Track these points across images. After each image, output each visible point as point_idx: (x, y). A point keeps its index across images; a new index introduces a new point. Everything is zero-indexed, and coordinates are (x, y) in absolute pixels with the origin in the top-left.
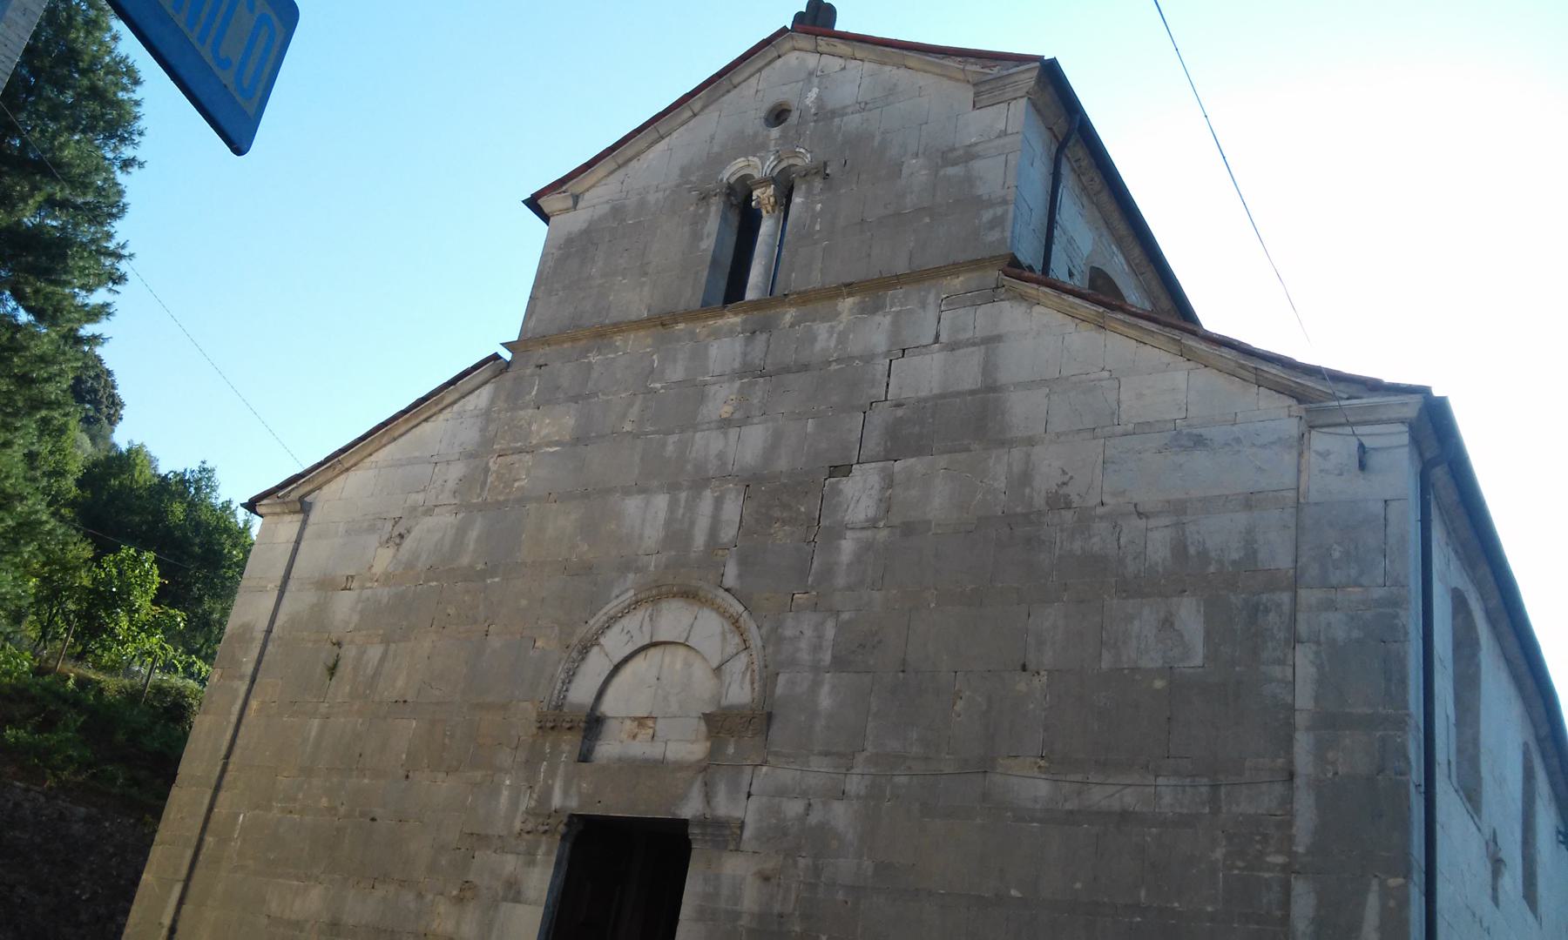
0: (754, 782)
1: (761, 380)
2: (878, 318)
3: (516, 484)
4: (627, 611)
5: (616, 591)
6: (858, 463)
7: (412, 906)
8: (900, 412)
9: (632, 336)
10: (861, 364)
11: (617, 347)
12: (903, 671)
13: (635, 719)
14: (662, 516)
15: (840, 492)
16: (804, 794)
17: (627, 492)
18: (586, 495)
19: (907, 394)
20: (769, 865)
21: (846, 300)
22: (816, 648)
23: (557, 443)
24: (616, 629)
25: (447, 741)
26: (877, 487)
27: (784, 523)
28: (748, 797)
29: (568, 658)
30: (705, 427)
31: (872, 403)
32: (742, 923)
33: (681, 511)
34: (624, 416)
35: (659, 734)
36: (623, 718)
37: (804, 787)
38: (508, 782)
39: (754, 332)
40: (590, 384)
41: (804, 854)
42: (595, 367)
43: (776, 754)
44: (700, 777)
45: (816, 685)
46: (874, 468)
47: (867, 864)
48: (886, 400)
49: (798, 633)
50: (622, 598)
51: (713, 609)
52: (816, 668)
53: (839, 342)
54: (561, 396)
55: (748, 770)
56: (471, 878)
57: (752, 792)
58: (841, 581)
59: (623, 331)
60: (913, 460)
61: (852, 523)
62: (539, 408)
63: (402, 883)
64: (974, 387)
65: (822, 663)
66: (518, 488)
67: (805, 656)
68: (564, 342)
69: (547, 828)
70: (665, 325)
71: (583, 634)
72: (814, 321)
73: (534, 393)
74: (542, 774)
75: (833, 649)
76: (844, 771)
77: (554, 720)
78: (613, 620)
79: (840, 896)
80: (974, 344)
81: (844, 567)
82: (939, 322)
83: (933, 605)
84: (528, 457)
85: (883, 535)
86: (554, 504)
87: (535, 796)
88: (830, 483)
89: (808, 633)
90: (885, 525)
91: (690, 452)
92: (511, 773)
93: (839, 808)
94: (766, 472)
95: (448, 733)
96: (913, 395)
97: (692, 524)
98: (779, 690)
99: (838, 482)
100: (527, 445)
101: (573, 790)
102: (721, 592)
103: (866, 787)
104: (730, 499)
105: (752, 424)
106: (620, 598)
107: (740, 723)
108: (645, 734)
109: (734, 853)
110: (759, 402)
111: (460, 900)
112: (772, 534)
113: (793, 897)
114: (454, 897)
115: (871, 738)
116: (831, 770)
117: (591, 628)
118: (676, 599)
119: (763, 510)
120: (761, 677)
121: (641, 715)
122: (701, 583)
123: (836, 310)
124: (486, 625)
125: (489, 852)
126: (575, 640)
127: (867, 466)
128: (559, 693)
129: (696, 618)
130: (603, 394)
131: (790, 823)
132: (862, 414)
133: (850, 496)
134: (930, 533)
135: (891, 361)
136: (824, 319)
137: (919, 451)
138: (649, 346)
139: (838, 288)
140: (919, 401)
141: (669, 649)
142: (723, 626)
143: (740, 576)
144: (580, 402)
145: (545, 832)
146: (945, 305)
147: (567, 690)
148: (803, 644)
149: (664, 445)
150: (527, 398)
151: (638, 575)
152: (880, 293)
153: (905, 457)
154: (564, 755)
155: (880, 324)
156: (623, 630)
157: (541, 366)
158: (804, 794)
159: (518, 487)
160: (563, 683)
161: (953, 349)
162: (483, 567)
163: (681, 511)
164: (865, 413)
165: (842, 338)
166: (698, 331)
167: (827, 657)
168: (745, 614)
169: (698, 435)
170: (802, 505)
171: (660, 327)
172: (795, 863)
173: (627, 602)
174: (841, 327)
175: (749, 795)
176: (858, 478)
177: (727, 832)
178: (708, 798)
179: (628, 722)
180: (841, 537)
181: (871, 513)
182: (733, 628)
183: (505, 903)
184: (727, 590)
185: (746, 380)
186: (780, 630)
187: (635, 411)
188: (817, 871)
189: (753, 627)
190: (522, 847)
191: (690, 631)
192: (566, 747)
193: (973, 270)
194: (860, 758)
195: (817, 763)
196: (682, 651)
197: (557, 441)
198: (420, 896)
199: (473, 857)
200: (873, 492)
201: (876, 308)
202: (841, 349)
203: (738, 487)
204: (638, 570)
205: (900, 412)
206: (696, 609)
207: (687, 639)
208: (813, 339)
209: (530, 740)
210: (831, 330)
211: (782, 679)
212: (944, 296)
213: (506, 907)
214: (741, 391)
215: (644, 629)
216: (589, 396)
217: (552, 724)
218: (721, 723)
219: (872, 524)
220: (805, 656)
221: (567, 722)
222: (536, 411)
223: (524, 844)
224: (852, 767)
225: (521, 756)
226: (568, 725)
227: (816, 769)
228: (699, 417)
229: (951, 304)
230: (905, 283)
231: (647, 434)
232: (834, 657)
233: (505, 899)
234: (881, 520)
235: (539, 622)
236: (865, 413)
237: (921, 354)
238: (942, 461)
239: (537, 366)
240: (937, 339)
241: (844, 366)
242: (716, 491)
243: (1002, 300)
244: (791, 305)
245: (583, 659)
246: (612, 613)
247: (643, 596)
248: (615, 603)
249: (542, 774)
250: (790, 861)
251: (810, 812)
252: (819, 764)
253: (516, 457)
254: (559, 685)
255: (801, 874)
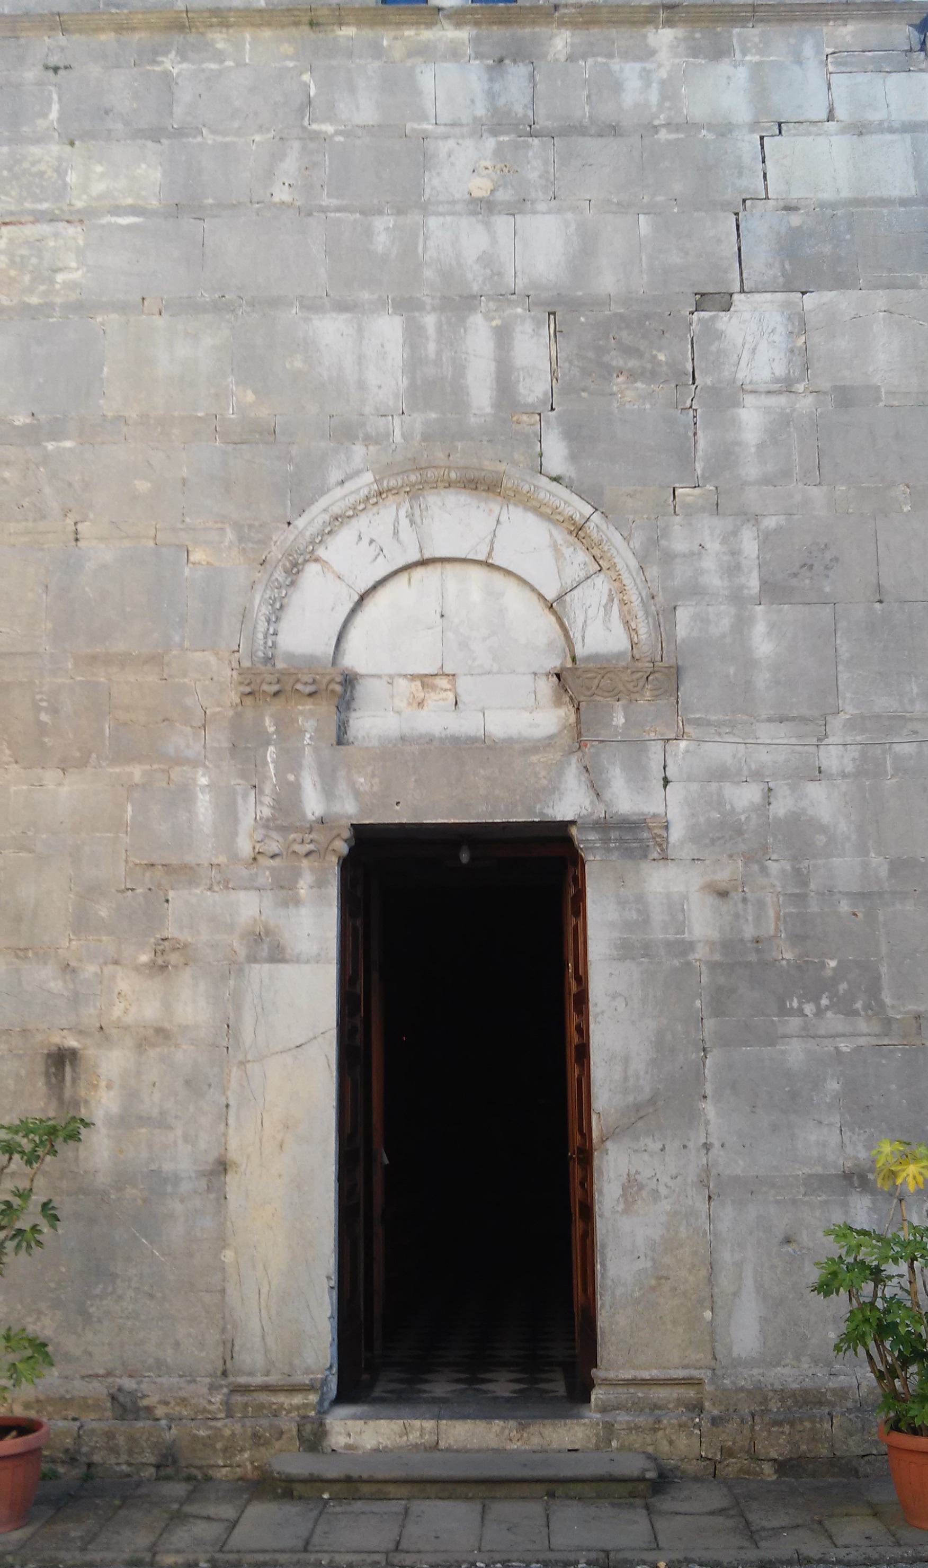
0: (669, 762)
1: (536, 141)
2: (724, 67)
3: (60, 277)
4: (361, 507)
5: (335, 475)
6: (742, 291)
7: (56, 985)
8: (795, 220)
9: (248, 36)
10: (711, 136)
11: (221, 52)
12: (881, 602)
13: (413, 677)
14: (396, 353)
15: (719, 336)
16: (757, 775)
17: (312, 307)
18: (220, 307)
19: (797, 193)
20: (723, 875)
21: (660, 31)
22: (733, 569)
23: (134, 210)
24: (346, 535)
25: (44, 717)
26: (781, 329)
27: (633, 376)
28: (665, 786)
29: (269, 580)
30: (441, 209)
31: (744, 201)
32: (697, 956)
33: (432, 347)
34: (270, 175)
35: (463, 698)
36: (391, 677)
37: (753, 767)
38: (203, 781)
39: (501, 61)
40: (178, 110)
41: (774, 857)
42: (179, 81)
43: (698, 723)
44: (574, 759)
45: (742, 624)
46: (772, 302)
47: (879, 864)
48: (767, 198)
49: (696, 548)
50: (350, 486)
51: (527, 508)
52: (737, 597)
53: (664, 97)
54: (120, 126)
55: (656, 749)
56: (171, 931)
57: (670, 777)
58: (751, 470)
59: (229, 26)
60: (834, 293)
61: (751, 383)
62: (72, 144)
63: (21, 954)
64: (905, 195)
65: (746, 591)
66: (65, 284)
67: (714, 581)
68: (98, 29)
69: (311, 847)
70: (318, 24)
71: (288, 543)
72: (610, 56)
73: (54, 115)
74: (271, 766)
75: (760, 571)
76: (814, 741)
77: (278, 682)
78: (339, 520)
79: (845, 907)
80: (892, 130)
81: (753, 450)
82: (829, 88)
83: (907, 508)
84: (71, 230)
85: (806, 403)
86: (156, 317)
87: (267, 800)
88: (699, 320)
89: (714, 546)
90: (806, 388)
91: (425, 249)
92: (204, 766)
93: (816, 792)
94: (580, 293)
95: (44, 704)
96: (811, 195)
97: (460, 369)
98: (681, 632)
99: (712, 319)
100: (66, 208)
101: (342, 787)
102: (544, 481)
103: (854, 760)
104: (523, 332)
105: (534, 212)
106: (347, 485)
107: (632, 681)
108: (439, 700)
109: (662, 862)
110: (540, 177)
111: (159, 968)
112: (613, 394)
113: (771, 913)
114: (145, 965)
115: (848, 695)
116: (794, 741)
117: (301, 533)
118: (451, 490)
119: (591, 355)
120: (647, 613)
121: (427, 672)
122: (502, 467)
123: (647, 45)
124: (70, 521)
125: (198, 891)
126: (275, 553)
127: (757, 297)
128: (266, 637)
129: (498, 521)
130: (214, 132)
131: (743, 818)
132: (734, 217)
133: (739, 341)
134: (881, 404)
135: (762, 138)
136: (626, 55)
137: (841, 282)
138: (287, 57)
139: (653, 9)
140: (822, 205)
141: (449, 567)
142: (551, 535)
143: (574, 457)
144: (163, 141)
145: (308, 854)
146: (837, 64)
147: (275, 634)
148: (709, 563)
149: (368, 232)
150: (41, 124)
151: (371, 448)
152: (719, 29)
153: (820, 288)
154: (308, 736)
155: (729, 78)
156: (360, 538)
157: (56, 69)
158: (757, 775)
159: (64, 282)
160: (269, 621)
161: (861, 134)
162: (28, 421)
163: (432, 347)
164: (737, 214)
165: (669, 92)
166: (385, 43)
167: (753, 583)
168: (596, 517)
169: (433, 222)
170: (660, 350)
171: (306, 28)
172: (764, 870)
173: (364, 492)
174: (663, 73)
175: (666, 781)
176: (746, 315)
177: (646, 835)
178: (597, 790)
179: (403, 683)
180: (736, 403)
181: (780, 370)
182: (572, 539)
183: (256, 967)
184: (556, 479)
185: (506, 138)
186: (663, 542)
187: (290, 165)
188: (801, 877)
189: (616, 538)
190: (265, 878)
191: (492, 543)
192: (309, 725)
193: (869, 18)
194: (836, 723)
195: (766, 732)
196: (477, 575)
197: (131, 206)
198: (67, 969)
199: (167, 901)
200: (776, 337)
201: (719, 52)
202: (670, 109)
203: (532, 313)
204: (368, 440)
205: (795, 220)
206: (496, 508)
207: (490, 554)
208: (617, 87)
209: (231, 713)
210: (646, 76)
211: (683, 615)
212: (830, 50)
213: (260, 972)
214: (499, 152)
215: (402, 535)
216: (180, 133)
217: (275, 688)
218: (596, 681)
219: (786, 386)
220: (714, 581)
221: (306, 684)
222: (68, 148)
223: (267, 873)
224: (826, 736)
225: (219, 738)
226: (309, 689)
227: (769, 741)
228: (427, 191)
229: (845, 64)
230: (762, 20)
231: (324, 210)
232: (764, 583)
233: (253, 959)
234: (798, 382)
235: (188, 520)
236: (737, 214)
237: (809, 134)
238: (881, 299)
239: (47, 68)
240: (830, 117)
241: (682, 136)
242: (493, 319)
243: (921, 70)
244: (562, 24)
245: (293, 583)
246: (336, 510)
247: (393, 483)
248: (338, 492)
249: (271, 766)
250: (755, 867)
251: (772, 800)
252: (781, 734)
253: (44, 229)
254: (262, 626)
255: (777, 883)
